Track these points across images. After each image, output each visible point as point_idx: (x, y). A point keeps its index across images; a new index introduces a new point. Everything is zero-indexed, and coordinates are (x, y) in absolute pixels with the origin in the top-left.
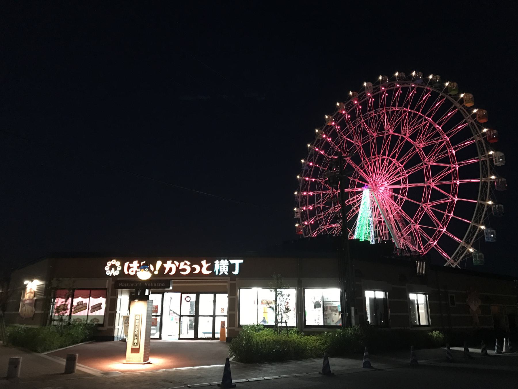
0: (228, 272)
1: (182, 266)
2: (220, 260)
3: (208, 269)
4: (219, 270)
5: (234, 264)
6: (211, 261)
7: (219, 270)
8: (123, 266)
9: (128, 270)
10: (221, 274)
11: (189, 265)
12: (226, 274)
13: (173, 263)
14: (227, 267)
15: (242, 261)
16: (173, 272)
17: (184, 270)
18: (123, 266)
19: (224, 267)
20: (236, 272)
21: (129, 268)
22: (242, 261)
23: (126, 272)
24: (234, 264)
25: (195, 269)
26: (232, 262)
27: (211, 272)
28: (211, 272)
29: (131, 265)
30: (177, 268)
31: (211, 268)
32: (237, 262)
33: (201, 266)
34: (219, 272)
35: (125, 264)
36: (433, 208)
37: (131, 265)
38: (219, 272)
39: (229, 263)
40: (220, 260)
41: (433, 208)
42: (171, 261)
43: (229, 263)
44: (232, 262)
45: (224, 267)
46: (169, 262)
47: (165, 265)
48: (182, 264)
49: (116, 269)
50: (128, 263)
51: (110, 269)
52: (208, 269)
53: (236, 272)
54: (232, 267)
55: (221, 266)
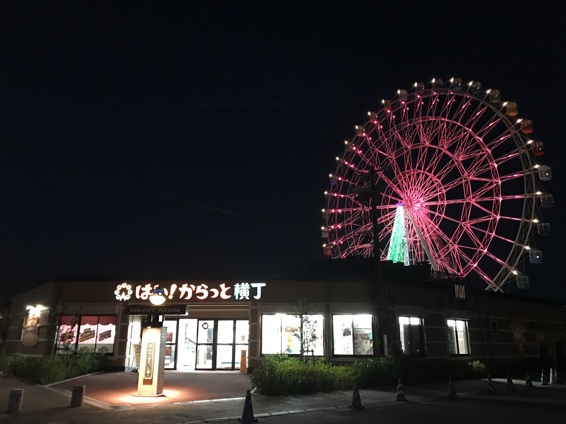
0: (249, 297)
1: (199, 290)
2: (240, 284)
3: (227, 293)
4: (239, 295)
5: (256, 288)
6: (231, 285)
7: (239, 295)
8: (134, 289)
9: (140, 295)
10: (241, 298)
11: (207, 289)
12: (247, 298)
13: (189, 286)
14: (248, 291)
15: (264, 285)
16: (189, 297)
17: (202, 294)
18: (134, 289)
19: (245, 291)
20: (258, 297)
21: (141, 292)
22: (264, 285)
23: (138, 297)
24: (256, 288)
25: (213, 294)
26: (254, 285)
27: (230, 296)
28: (230, 296)
29: (143, 289)
30: (194, 292)
31: (231, 292)
32: (259, 286)
33: (220, 290)
34: (239, 296)
35: (137, 288)
36: (473, 227)
37: (143, 289)
38: (239, 296)
39: (251, 286)
40: (240, 284)
41: (473, 227)
42: (187, 285)
43: (251, 286)
44: (254, 285)
45: (245, 291)
46: (185, 286)
47: (180, 289)
48: (199, 287)
49: (126, 294)
50: (140, 286)
51: (121, 294)
52: (227, 293)
53: (258, 297)
54: (253, 291)
55: (241, 290)
